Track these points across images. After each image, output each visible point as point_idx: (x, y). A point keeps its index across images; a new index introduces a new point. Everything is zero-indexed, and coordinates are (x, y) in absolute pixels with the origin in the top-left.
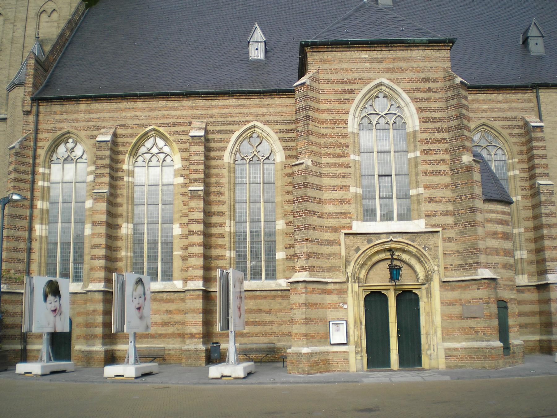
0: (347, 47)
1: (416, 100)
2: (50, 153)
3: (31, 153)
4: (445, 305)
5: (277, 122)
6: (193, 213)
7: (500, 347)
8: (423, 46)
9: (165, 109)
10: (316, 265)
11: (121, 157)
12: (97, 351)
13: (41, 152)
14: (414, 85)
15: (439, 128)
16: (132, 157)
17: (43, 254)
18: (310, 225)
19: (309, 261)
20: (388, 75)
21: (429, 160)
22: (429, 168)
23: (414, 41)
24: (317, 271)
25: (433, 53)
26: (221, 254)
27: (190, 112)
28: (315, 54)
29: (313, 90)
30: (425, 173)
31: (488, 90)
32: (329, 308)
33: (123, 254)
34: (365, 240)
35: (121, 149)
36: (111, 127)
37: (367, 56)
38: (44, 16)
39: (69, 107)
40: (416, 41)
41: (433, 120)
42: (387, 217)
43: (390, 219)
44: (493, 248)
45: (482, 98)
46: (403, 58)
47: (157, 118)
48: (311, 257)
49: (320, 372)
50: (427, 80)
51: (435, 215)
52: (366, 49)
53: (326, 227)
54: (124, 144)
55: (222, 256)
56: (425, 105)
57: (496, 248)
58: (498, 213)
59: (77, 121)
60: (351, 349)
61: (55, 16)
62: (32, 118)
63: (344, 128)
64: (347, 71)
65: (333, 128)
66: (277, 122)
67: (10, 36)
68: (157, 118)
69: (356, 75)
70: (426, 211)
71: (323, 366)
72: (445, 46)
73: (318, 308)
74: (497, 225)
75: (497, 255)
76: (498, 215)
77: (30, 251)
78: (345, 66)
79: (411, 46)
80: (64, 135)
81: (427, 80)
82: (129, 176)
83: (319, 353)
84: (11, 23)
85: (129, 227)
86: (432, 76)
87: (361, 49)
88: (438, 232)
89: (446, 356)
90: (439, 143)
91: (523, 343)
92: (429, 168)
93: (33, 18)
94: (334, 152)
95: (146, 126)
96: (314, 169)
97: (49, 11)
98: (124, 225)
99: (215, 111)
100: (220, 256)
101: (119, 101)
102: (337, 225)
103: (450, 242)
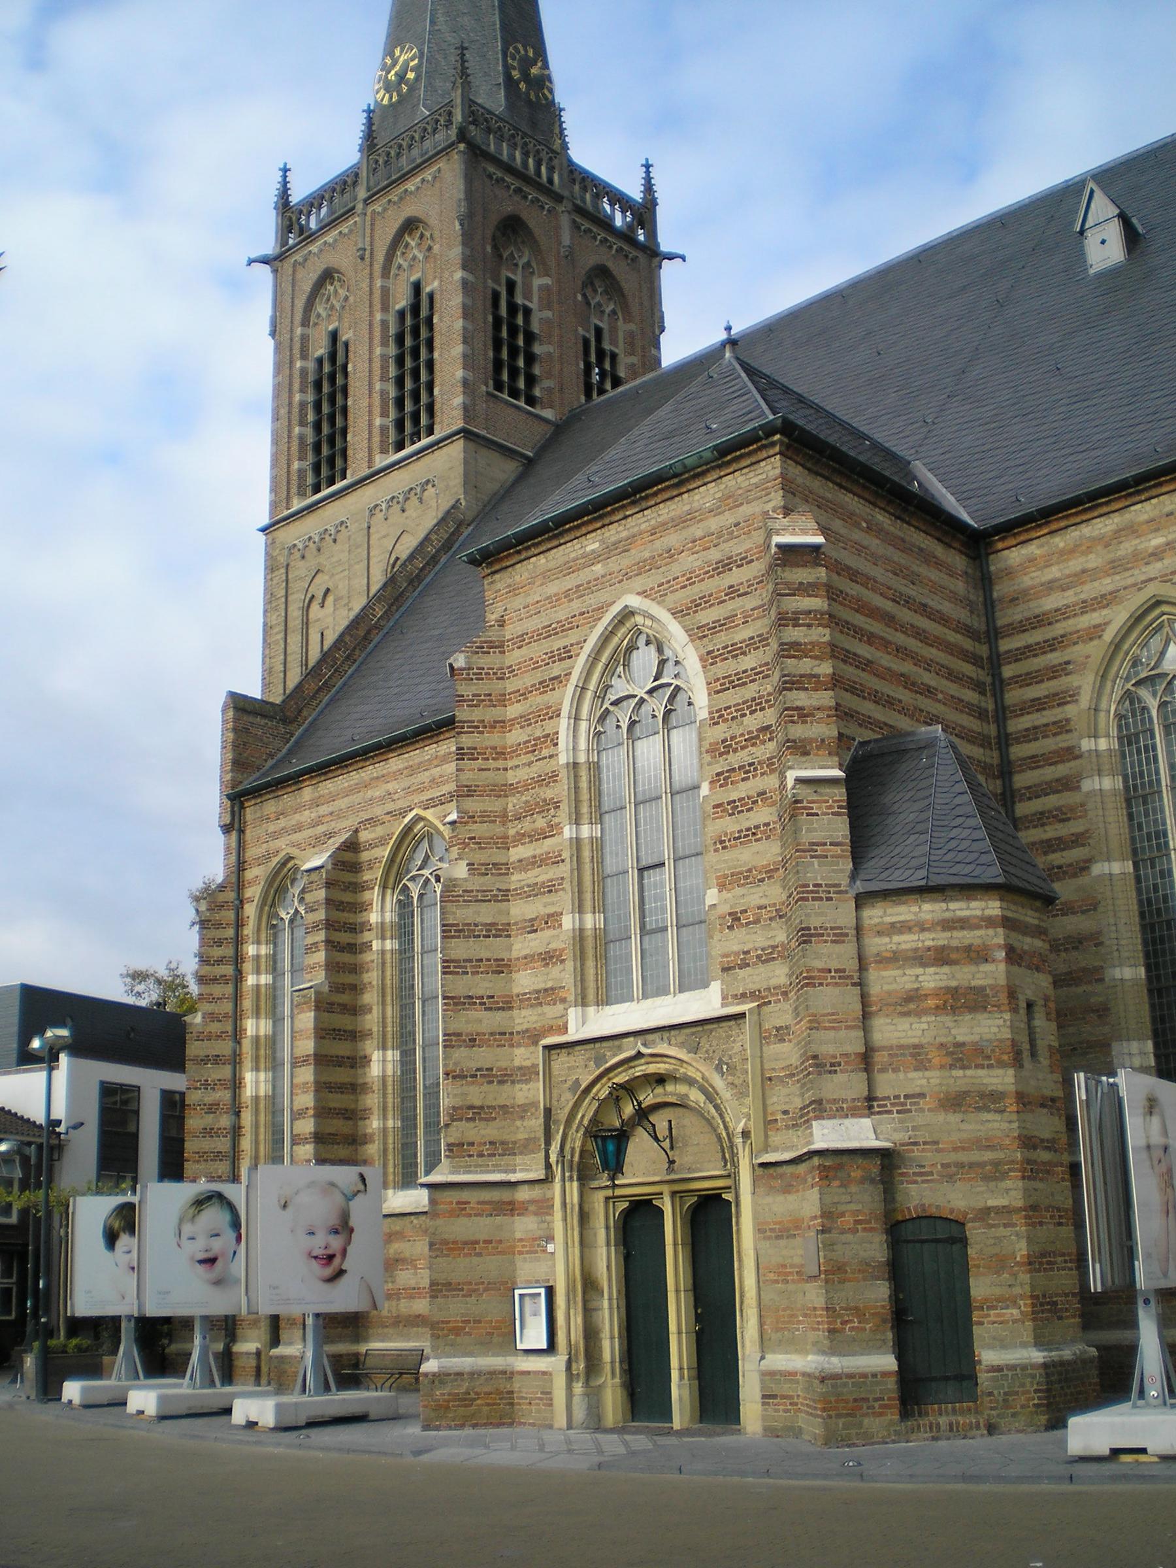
0: (556, 537)
2: (267, 908)
3: (230, 915)
4: (769, 1238)
7: (885, 1374)
8: (713, 468)
9: (435, 762)
10: (477, 1140)
11: (367, 895)
12: (290, 1357)
14: (695, 591)
15: (754, 699)
16: (389, 891)
17: (262, 1137)
18: (459, 1035)
20: (639, 583)
21: (729, 803)
22: (731, 825)
23: (685, 467)
24: (481, 1155)
25: (740, 479)
28: (497, 576)
29: (480, 675)
30: (722, 842)
31: (1160, 484)
32: (521, 1253)
33: (375, 1124)
34: (589, 1059)
37: (597, 545)
40: (688, 462)
43: (662, 991)
44: (901, 1047)
45: (1146, 517)
46: (673, 520)
48: (461, 1120)
49: (474, 1426)
51: (745, 965)
52: (591, 528)
53: (518, 1033)
57: (915, 1046)
58: (923, 930)
59: (298, 828)
60: (556, 1364)
63: (551, 756)
64: (554, 601)
65: (530, 764)
69: (576, 606)
70: (727, 956)
71: (486, 1408)
72: (764, 447)
73: (479, 1255)
74: (920, 971)
75: (916, 1069)
76: (927, 935)
77: (236, 1132)
78: (553, 588)
79: (687, 480)
80: (284, 864)
81: (724, 566)
83: (472, 1374)
85: (390, 1058)
87: (584, 530)
88: (742, 1015)
89: (764, 1397)
90: (754, 745)
91: (1093, 1352)
92: (731, 825)
94: (532, 826)
95: (403, 813)
96: (477, 883)
98: (376, 1056)
101: (361, 764)
102: (537, 1025)
103: (782, 1040)
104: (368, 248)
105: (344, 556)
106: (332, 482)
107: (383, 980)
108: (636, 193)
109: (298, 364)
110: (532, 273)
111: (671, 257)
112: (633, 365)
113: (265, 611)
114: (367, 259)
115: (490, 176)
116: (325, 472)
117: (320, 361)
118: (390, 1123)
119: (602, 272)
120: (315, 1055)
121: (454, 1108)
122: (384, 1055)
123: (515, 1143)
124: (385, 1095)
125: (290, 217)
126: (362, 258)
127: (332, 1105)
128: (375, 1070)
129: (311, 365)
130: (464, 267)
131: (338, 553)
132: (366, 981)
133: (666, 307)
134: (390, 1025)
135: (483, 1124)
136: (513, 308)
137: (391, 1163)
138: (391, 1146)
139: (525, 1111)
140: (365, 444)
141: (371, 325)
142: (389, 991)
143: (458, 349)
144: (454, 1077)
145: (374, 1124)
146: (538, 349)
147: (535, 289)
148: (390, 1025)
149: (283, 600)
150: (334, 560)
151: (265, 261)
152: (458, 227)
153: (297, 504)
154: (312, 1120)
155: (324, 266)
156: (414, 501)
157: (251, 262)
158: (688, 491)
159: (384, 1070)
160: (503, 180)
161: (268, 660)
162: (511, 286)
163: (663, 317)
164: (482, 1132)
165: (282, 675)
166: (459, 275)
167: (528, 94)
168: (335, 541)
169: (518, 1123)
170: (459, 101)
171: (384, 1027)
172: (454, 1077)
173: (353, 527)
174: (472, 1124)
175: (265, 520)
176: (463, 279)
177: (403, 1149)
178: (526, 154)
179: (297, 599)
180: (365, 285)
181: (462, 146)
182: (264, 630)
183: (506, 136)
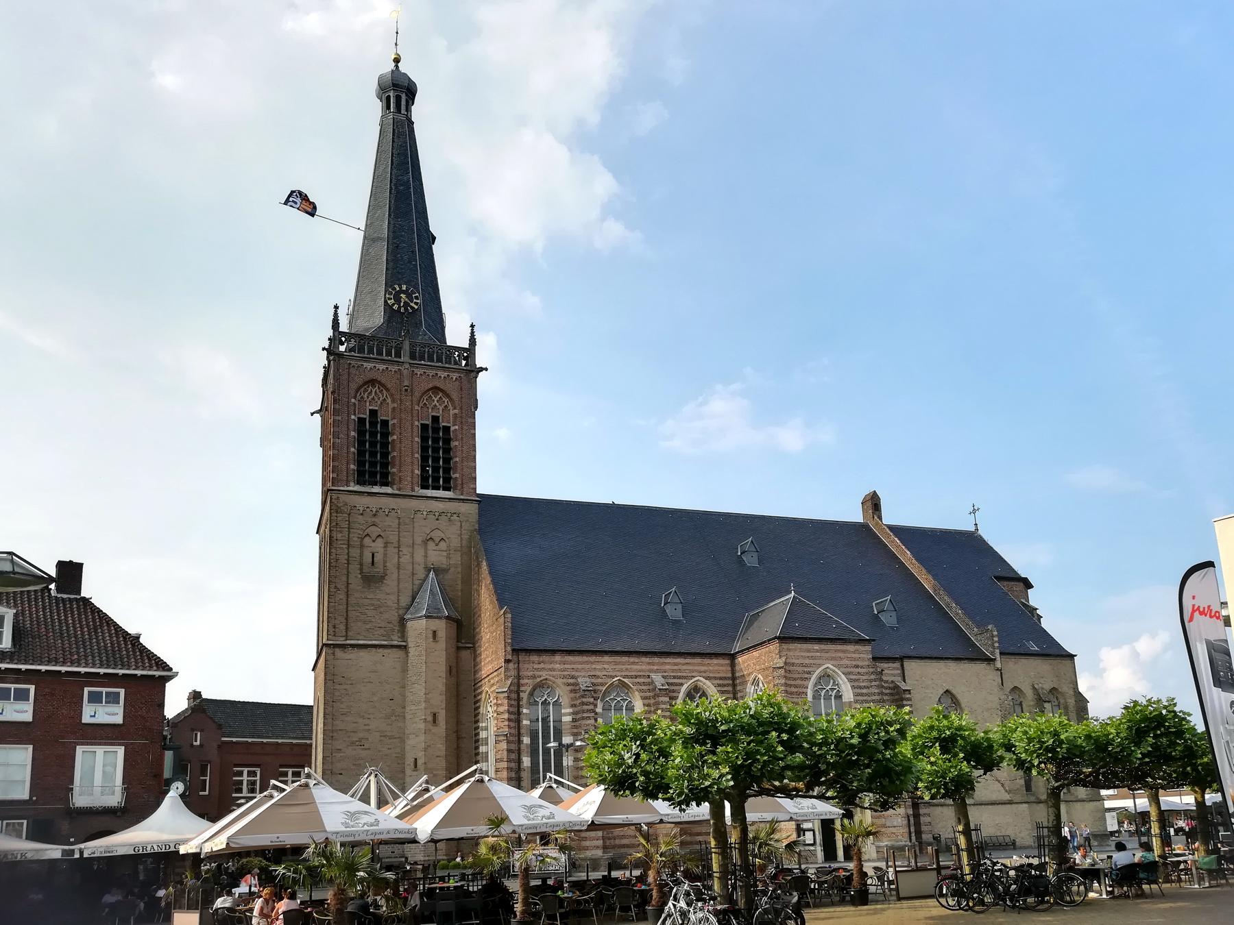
1: (850, 680)
5: (715, 678)
13: (524, 696)
27: (648, 667)
38: (431, 545)
39: (545, 658)
41: (862, 695)
42: (28, 592)
47: (621, 670)
50: (857, 666)
56: (856, 684)
61: (443, 545)
62: (511, 665)
64: (804, 657)
66: (715, 678)
68: (621, 670)
81: (857, 666)
86: (860, 663)
97: (437, 540)
99: (667, 667)
111: (481, 369)
162: (435, 419)
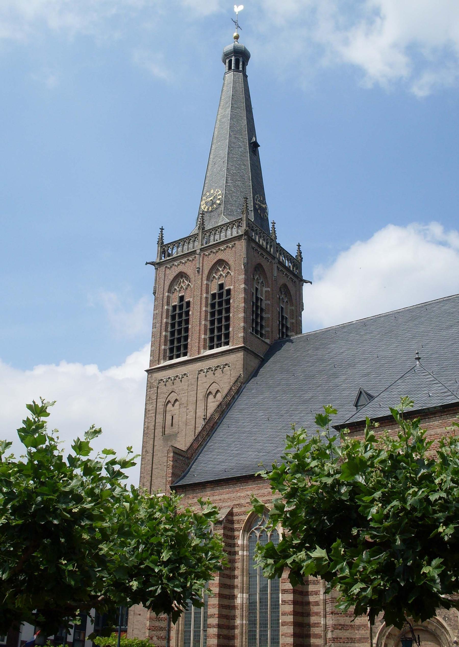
6: (284, 584)
10: (342, 637)
11: (236, 533)
19: (334, 632)
24: (344, 643)
26: (317, 622)
35: (236, 526)
36: (229, 507)
38: (211, 397)
48: (337, 629)
54: (238, 522)
55: (318, 623)
67: (184, 419)
82: (243, 551)
84: (185, 407)
85: (245, 597)
93: (201, 400)
98: (239, 595)
100: (315, 623)
104: (201, 268)
105: (186, 387)
106: (178, 356)
107: (243, 566)
108: (294, 254)
109: (166, 307)
110: (263, 286)
111: (306, 282)
112: (293, 323)
113: (146, 404)
114: (201, 273)
115: (253, 248)
116: (175, 353)
117: (174, 307)
118: (244, 622)
119: (285, 286)
120: (219, 594)
121: (335, 625)
122: (243, 596)
123: (355, 639)
124: (243, 611)
125: (164, 248)
126: (198, 271)
127: (223, 613)
128: (238, 601)
129: (170, 308)
130: (245, 283)
131: (184, 385)
132: (236, 566)
133: (304, 301)
134: (245, 584)
135: (344, 631)
136: (257, 298)
137: (244, 638)
138: (244, 631)
139: (360, 627)
140: (197, 344)
141: (201, 298)
142: (245, 571)
143: (242, 315)
144: (335, 614)
145: (238, 622)
146: (264, 315)
147: (264, 292)
148: (245, 584)
149: (155, 400)
150: (180, 388)
151: (152, 264)
152: (243, 268)
153: (163, 364)
154: (217, 619)
155: (179, 271)
156: (219, 371)
157: (147, 263)
158: (428, 418)
159: (243, 601)
160: (257, 250)
161: (147, 424)
163: (303, 305)
164: (345, 634)
165: (153, 431)
166: (243, 286)
167: (260, 215)
168: (181, 381)
169: (356, 632)
170: (244, 219)
171: (243, 585)
172: (335, 614)
173: (190, 377)
174: (341, 631)
175: (148, 368)
176: (245, 288)
177: (249, 632)
178: (267, 243)
179: (161, 401)
180: (199, 282)
181: (246, 237)
182: (145, 411)
183: (258, 233)
